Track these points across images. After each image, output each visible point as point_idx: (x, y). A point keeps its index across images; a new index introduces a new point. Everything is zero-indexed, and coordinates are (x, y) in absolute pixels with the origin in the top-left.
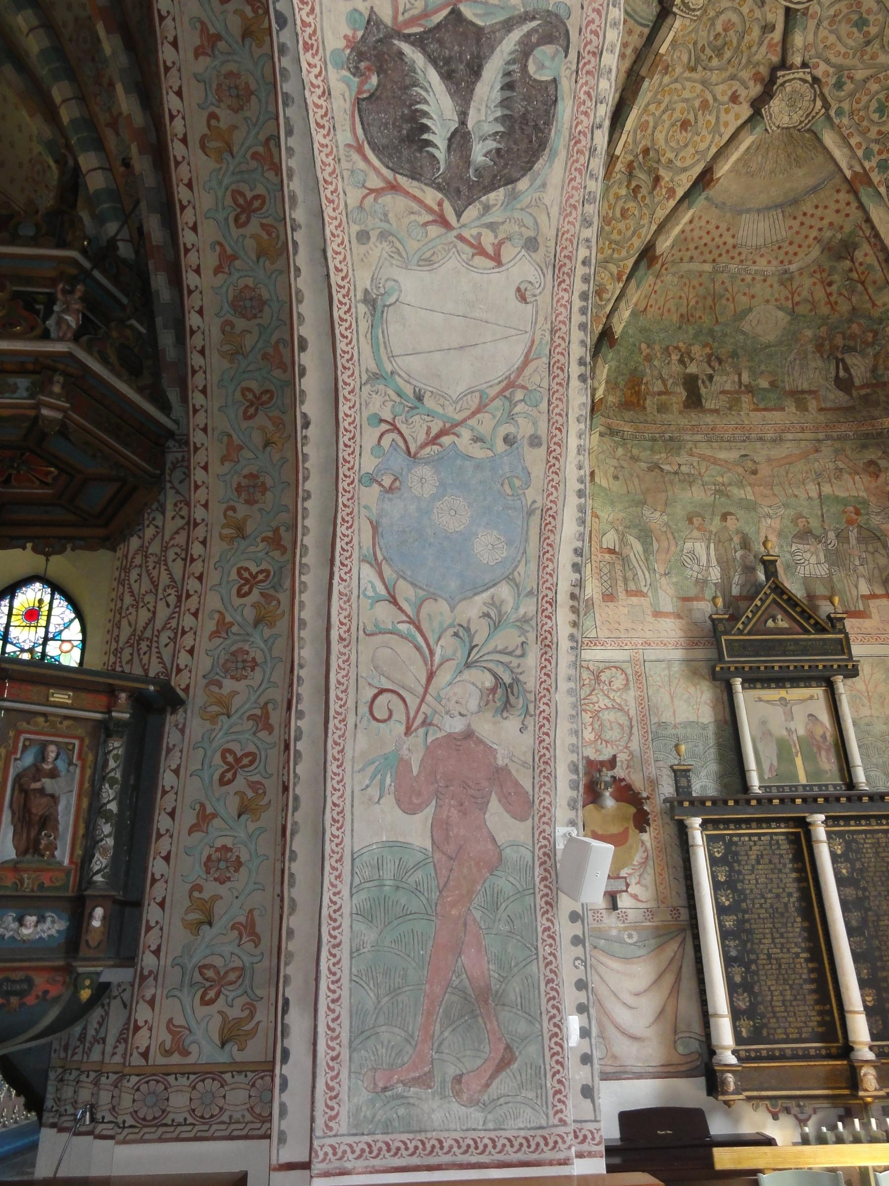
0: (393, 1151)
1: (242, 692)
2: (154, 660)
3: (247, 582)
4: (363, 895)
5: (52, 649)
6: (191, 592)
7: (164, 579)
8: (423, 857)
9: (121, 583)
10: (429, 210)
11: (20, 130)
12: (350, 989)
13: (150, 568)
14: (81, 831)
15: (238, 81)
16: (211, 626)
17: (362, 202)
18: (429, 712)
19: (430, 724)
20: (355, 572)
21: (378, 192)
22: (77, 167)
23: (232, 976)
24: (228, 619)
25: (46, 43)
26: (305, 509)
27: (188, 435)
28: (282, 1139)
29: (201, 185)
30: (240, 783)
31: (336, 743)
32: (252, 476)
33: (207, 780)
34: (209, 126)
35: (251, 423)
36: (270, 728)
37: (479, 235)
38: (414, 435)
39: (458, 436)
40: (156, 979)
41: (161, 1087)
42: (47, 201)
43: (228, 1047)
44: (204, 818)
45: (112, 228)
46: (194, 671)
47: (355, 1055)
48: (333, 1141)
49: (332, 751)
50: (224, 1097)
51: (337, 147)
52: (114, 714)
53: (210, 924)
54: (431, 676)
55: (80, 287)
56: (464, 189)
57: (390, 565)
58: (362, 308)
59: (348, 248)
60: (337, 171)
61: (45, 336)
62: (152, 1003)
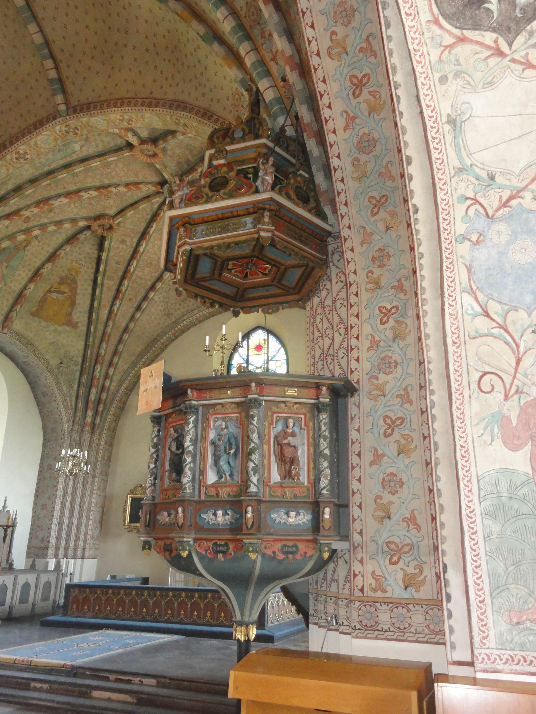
0: (528, 662)
1: (390, 381)
2: (337, 367)
3: (386, 314)
4: (488, 502)
5: (272, 366)
6: (353, 325)
7: (336, 320)
8: (527, 478)
9: (312, 324)
10: (489, 47)
11: (225, 79)
12: (487, 561)
13: (327, 314)
14: (312, 466)
15: (346, 6)
16: (367, 343)
17: (440, 56)
18: (520, 384)
19: (522, 392)
20: (458, 299)
21: (451, 47)
22: (258, 90)
23: (406, 549)
24: (377, 338)
25: (234, 23)
26: (420, 265)
27: (339, 232)
28: (453, 647)
29: (331, 78)
30: (396, 435)
31: (458, 408)
32: (381, 250)
33: (376, 435)
34: (331, 40)
35: (376, 217)
36: (410, 402)
37: (527, 54)
38: (491, 204)
39: (523, 198)
40: (362, 548)
41: (373, 609)
42: (245, 115)
43: (409, 589)
44: (377, 457)
45: (281, 120)
46: (361, 373)
47: (494, 600)
48: (487, 651)
49: (456, 414)
50: (411, 618)
51: (421, 25)
52: (321, 399)
53: (389, 518)
54: (518, 361)
55: (271, 159)
56: (513, 26)
57: (482, 292)
58: (447, 127)
59: (433, 90)
60: (422, 41)
61: (257, 191)
62: (361, 562)
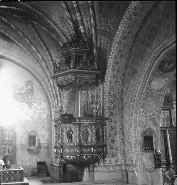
53: (112, 149)
